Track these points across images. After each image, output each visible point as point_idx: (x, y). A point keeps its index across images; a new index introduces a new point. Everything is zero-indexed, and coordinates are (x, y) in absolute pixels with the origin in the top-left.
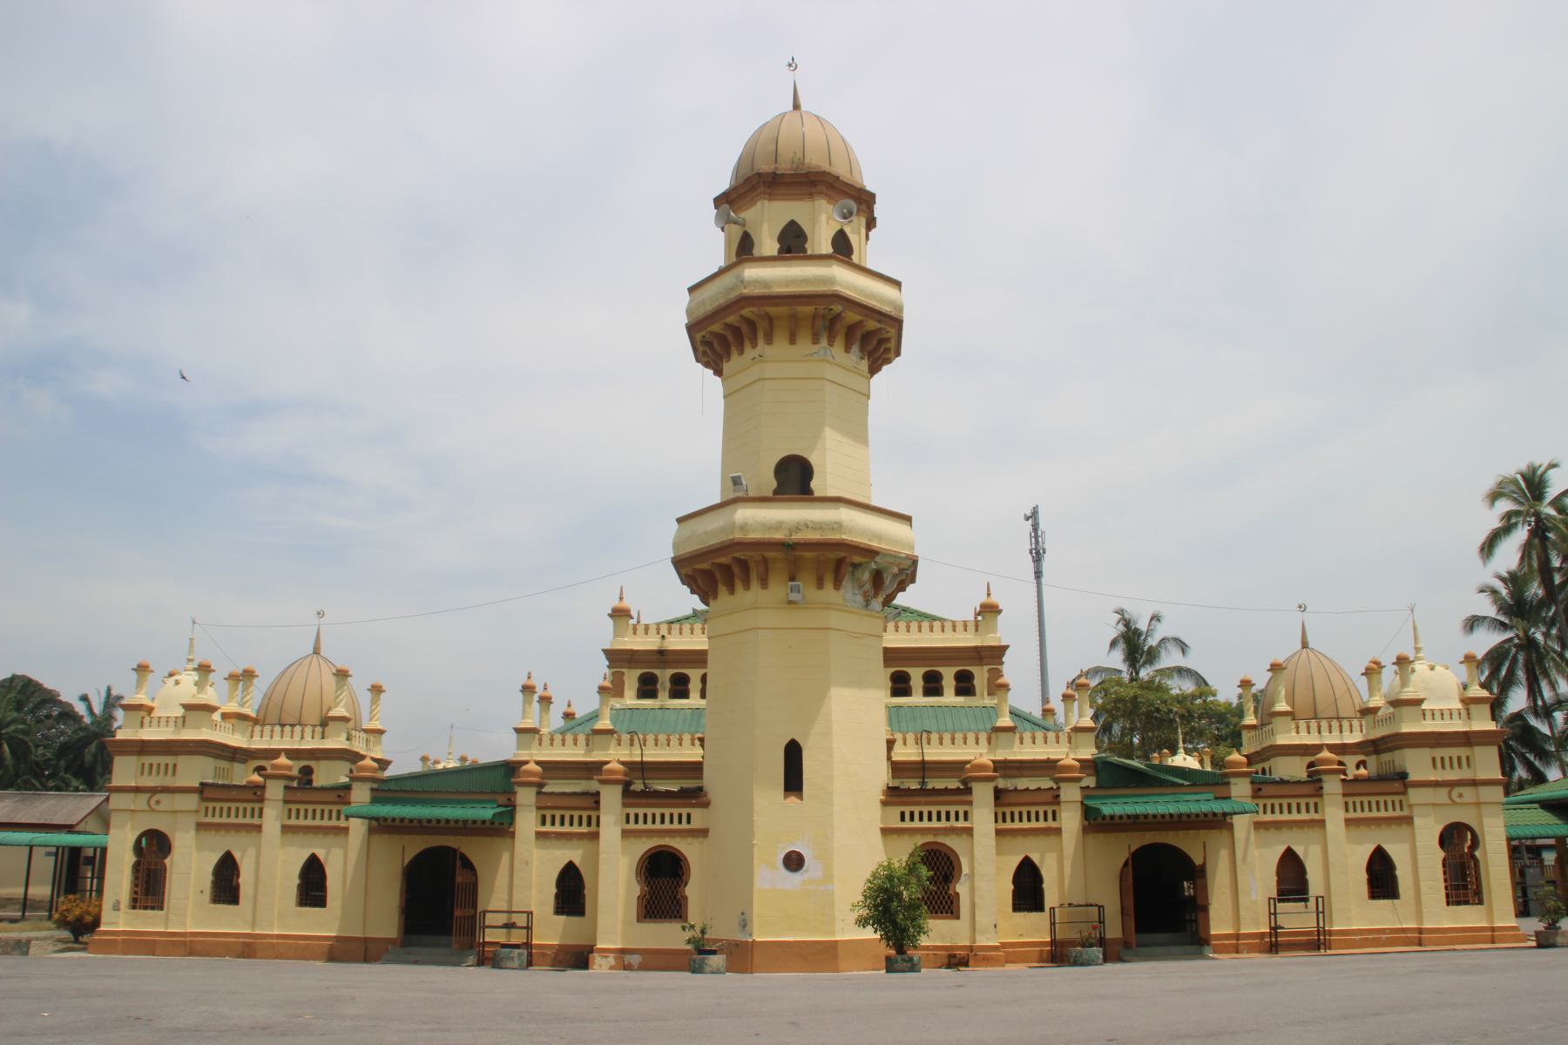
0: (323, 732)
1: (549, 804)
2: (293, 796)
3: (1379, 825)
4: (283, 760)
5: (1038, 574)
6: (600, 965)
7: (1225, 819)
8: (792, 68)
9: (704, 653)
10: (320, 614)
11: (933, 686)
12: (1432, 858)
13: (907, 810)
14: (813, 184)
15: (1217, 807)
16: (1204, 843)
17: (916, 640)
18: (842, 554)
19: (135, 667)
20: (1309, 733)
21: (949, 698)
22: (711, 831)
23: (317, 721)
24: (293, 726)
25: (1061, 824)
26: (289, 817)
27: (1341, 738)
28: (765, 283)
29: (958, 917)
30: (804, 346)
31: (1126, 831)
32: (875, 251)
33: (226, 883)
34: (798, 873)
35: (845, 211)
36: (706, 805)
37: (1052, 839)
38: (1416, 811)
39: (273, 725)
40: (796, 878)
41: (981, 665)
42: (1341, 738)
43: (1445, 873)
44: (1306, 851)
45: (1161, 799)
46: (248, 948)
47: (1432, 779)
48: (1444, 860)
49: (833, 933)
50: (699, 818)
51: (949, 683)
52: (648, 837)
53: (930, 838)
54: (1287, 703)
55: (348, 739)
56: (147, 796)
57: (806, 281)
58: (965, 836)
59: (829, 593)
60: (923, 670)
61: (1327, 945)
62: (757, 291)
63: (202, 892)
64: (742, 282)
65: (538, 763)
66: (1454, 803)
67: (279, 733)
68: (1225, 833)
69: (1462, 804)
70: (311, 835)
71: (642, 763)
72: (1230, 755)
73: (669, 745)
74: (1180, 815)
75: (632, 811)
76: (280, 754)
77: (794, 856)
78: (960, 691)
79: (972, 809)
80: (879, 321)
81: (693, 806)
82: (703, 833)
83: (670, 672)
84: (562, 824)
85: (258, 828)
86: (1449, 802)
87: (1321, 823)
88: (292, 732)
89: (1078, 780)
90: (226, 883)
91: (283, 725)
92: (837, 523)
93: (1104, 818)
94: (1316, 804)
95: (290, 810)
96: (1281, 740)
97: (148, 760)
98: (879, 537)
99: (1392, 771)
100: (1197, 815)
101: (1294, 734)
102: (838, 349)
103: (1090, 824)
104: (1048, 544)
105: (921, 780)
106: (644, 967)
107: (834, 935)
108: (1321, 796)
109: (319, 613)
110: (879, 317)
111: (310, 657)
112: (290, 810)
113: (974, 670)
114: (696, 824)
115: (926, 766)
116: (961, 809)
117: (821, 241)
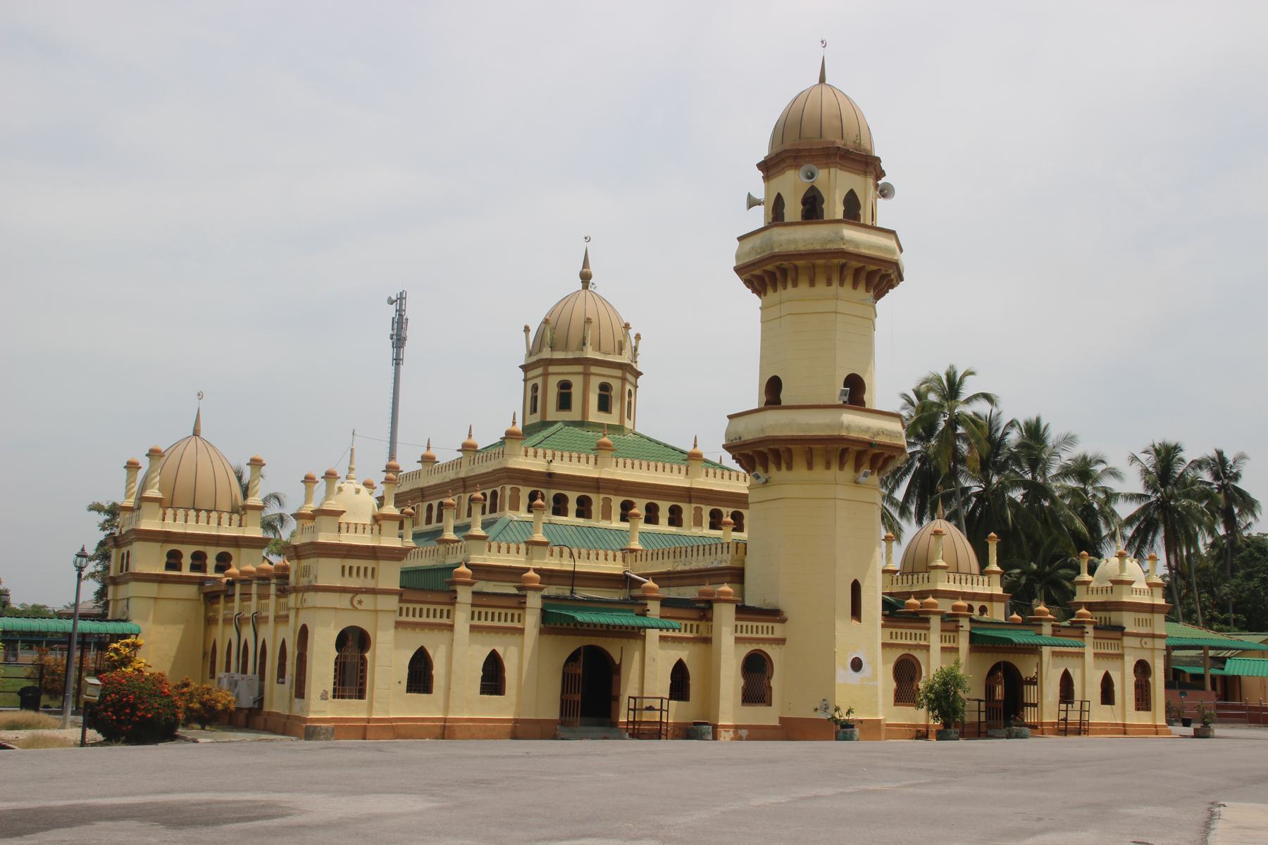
0: (241, 520)
1: (669, 615)
2: (669, 612)
3: (498, 633)
5: (397, 361)
6: (725, 736)
7: (639, 632)
8: (200, 397)
10: (200, 395)
11: (584, 509)
13: (894, 630)
14: (783, 160)
15: (639, 621)
16: (622, 648)
17: (728, 486)
18: (845, 446)
19: (249, 462)
20: (955, 583)
21: (663, 527)
24: (209, 511)
25: (524, 624)
27: (973, 588)
28: (857, 244)
29: (770, 705)
30: (821, 288)
31: (570, 634)
34: (859, 673)
35: (886, 191)
37: (517, 638)
38: (1126, 651)
39: (187, 509)
40: (857, 675)
41: (598, 493)
42: (973, 588)
43: (335, 678)
44: (434, 654)
45: (1023, 633)
47: (1135, 631)
48: (337, 659)
49: (876, 714)
50: (779, 630)
51: (664, 515)
52: (749, 643)
53: (906, 651)
54: (159, 490)
57: (879, 248)
58: (924, 651)
59: (784, 474)
61: (1086, 732)
62: (851, 249)
63: (400, 682)
64: (842, 239)
65: (536, 570)
68: (639, 642)
71: (574, 572)
72: (909, 599)
73: (588, 558)
74: (608, 626)
75: (739, 623)
76: (911, 595)
77: (857, 660)
78: (580, 514)
79: (929, 633)
82: (781, 641)
83: (554, 492)
86: (351, 607)
87: (451, 628)
88: (209, 517)
89: (541, 589)
93: (1016, 644)
99: (1108, 623)
100: (627, 627)
101: (947, 583)
102: (847, 290)
103: (545, 626)
104: (411, 333)
105: (571, 588)
106: (749, 738)
107: (877, 716)
113: (593, 496)
114: (777, 635)
115: (576, 575)
116: (923, 632)
117: (836, 208)
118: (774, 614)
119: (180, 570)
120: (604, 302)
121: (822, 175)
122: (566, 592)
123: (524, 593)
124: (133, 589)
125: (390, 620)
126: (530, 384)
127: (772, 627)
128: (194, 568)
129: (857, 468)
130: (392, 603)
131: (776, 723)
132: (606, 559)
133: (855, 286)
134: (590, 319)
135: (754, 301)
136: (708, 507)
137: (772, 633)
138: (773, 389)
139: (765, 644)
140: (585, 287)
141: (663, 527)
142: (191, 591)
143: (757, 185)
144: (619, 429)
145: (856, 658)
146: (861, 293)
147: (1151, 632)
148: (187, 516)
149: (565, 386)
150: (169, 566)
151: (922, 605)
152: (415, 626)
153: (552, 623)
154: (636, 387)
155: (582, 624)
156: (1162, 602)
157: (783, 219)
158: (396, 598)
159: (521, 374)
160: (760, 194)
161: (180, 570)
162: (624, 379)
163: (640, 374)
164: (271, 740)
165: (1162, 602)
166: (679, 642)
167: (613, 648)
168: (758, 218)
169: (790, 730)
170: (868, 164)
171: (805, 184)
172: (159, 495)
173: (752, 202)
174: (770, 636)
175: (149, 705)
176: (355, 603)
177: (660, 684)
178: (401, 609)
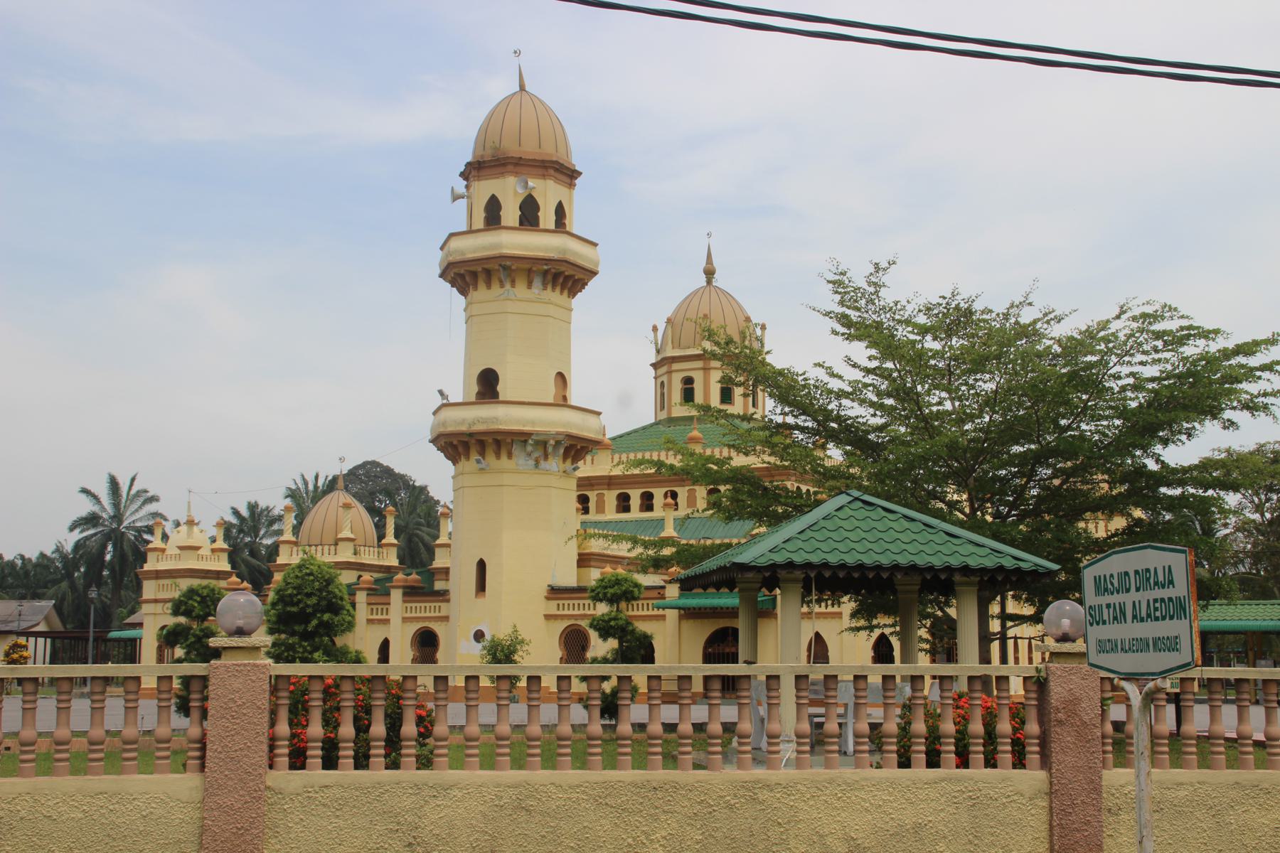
2: (374, 599)
13: (561, 602)
14: (504, 165)
22: (451, 618)
23: (332, 542)
24: (316, 546)
26: (406, 612)
30: (496, 290)
36: (448, 601)
50: (445, 609)
53: (572, 622)
55: (355, 554)
56: (162, 604)
59: (504, 462)
70: (654, 622)
75: (409, 605)
77: (479, 633)
80: (546, 264)
81: (442, 601)
82: (446, 618)
85: (387, 622)
92: (495, 418)
95: (372, 609)
97: (161, 582)
98: (533, 423)
109: (340, 459)
110: (544, 262)
112: (372, 609)
114: (443, 614)
117: (511, 214)
120: (728, 297)
127: (440, 607)
129: (482, 453)
133: (489, 285)
134: (668, 319)
135: (460, 300)
136: (661, 489)
137: (439, 612)
138: (488, 384)
139: (430, 621)
140: (709, 282)
141: (635, 513)
145: (479, 630)
146: (555, 296)
147: (154, 597)
149: (688, 381)
157: (537, 224)
159: (652, 372)
166: (824, 618)
168: (458, 217)
170: (569, 175)
171: (522, 193)
174: (437, 614)
175: (367, 719)
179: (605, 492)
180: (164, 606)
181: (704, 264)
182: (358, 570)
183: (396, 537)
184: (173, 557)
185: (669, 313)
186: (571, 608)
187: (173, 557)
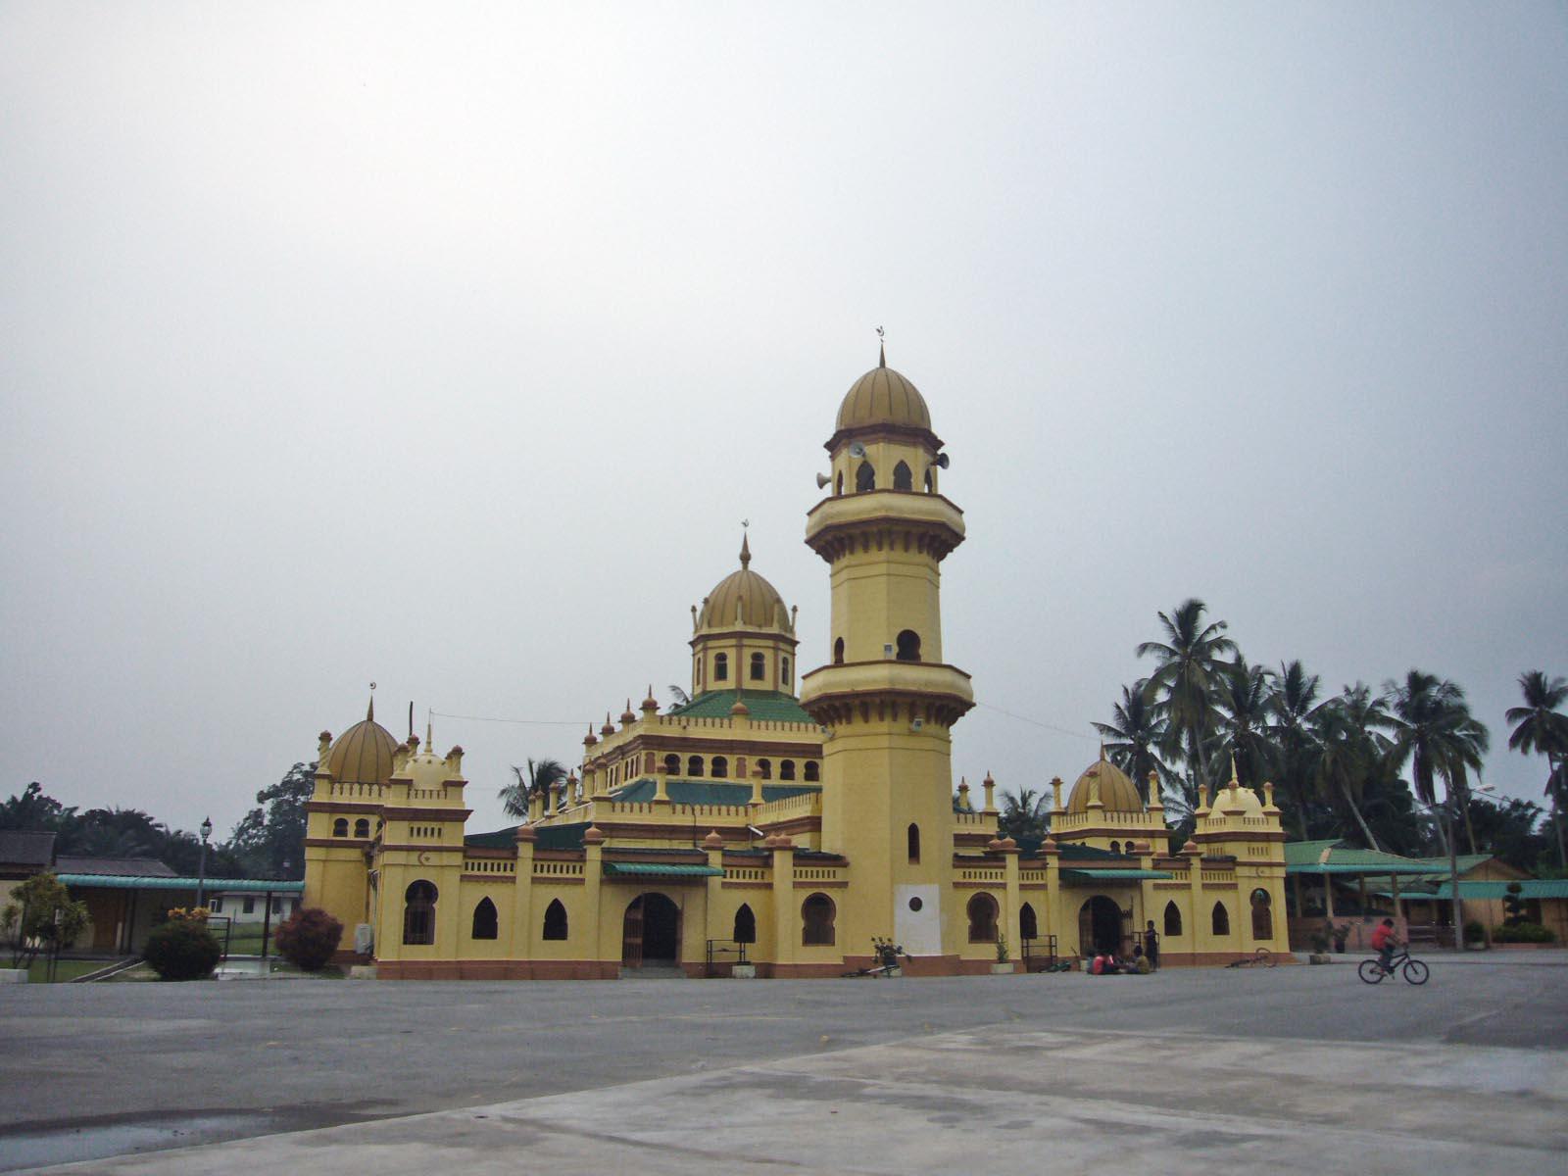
2: (729, 861)
4: (714, 835)
9: (820, 747)
12: (1247, 909)
13: (967, 870)
24: (371, 784)
27: (350, 800)
29: (833, 944)
32: (946, 482)
33: (485, 922)
46: (506, 971)
50: (840, 875)
53: (815, 890)
60: (781, 759)
66: (423, 865)
67: (358, 792)
69: (1264, 877)
71: (695, 826)
75: (798, 869)
82: (844, 885)
84: (738, 877)
85: (513, 880)
89: (601, 843)
90: (485, 922)
91: (361, 784)
94: (1001, 873)
96: (315, 798)
108: (585, 861)
111: (365, 724)
114: (839, 879)
116: (999, 871)
117: (884, 478)
118: (837, 861)
119: (346, 835)
121: (872, 450)
122: (689, 846)
123: (706, 852)
124: (387, 857)
125: (453, 877)
126: (697, 658)
128: (358, 833)
130: (457, 859)
131: (840, 962)
132: (729, 814)
137: (834, 877)
142: (355, 854)
143: (825, 466)
144: (774, 694)
148: (351, 789)
149: (721, 658)
150: (337, 833)
151: (1002, 845)
152: (1166, 887)
153: (611, 877)
154: (794, 655)
155: (623, 873)
156: (1280, 830)
158: (460, 855)
159: (690, 649)
160: (827, 473)
161: (346, 835)
162: (776, 649)
163: (797, 643)
164: (503, 992)
165: (1280, 830)
167: (675, 896)
169: (855, 969)
171: (857, 459)
172: (328, 772)
173: (822, 483)
174: (832, 880)
176: (1259, 872)
177: (724, 928)
178: (467, 864)
179: (746, 757)
180: (421, 855)
181: (739, 550)
182: (1109, 836)
183: (668, 792)
184: (427, 793)
185: (707, 594)
186: (747, 876)
187: (427, 793)
